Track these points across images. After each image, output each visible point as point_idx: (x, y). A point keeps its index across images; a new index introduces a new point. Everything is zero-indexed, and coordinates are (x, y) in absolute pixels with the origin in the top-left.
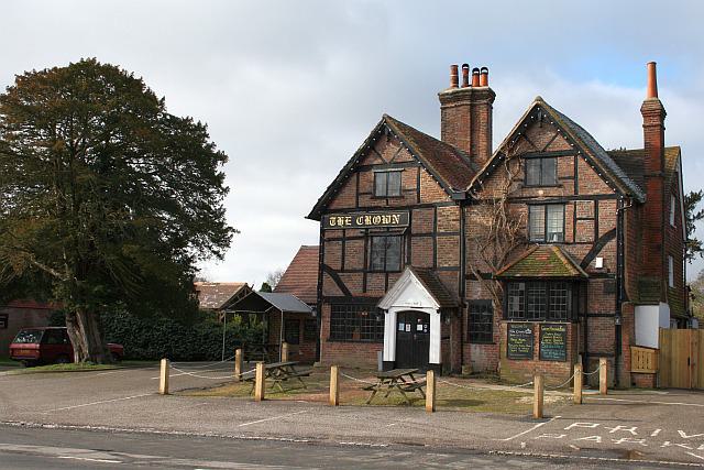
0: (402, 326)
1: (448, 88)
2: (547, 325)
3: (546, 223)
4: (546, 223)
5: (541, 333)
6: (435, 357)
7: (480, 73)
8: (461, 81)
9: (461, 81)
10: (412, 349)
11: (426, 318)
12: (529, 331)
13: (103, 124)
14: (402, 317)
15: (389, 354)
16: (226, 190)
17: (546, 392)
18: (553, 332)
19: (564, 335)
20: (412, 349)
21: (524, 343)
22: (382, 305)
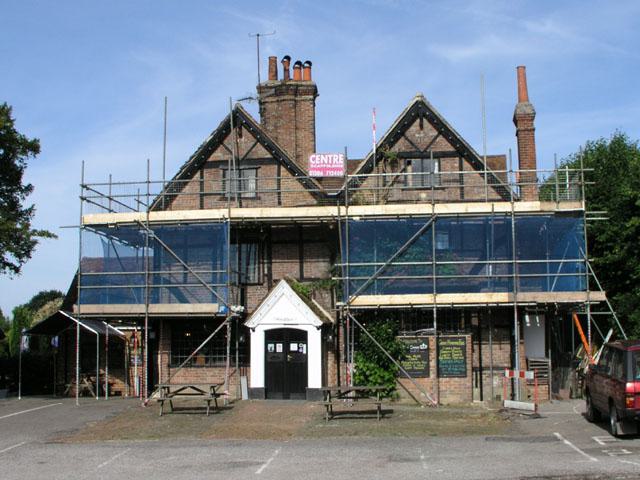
0: (271, 346)
1: (265, 79)
2: (445, 339)
3: (339, 377)
4: (339, 377)
5: (439, 348)
6: (314, 380)
7: (304, 66)
8: (281, 75)
9: (281, 75)
10: (286, 375)
11: (301, 336)
12: (424, 346)
13: (628, 282)
14: (272, 336)
15: (257, 376)
16: (29, 188)
17: (442, 343)
18: (452, 346)
19: (463, 348)
20: (286, 375)
21: (419, 360)
22: (249, 324)
